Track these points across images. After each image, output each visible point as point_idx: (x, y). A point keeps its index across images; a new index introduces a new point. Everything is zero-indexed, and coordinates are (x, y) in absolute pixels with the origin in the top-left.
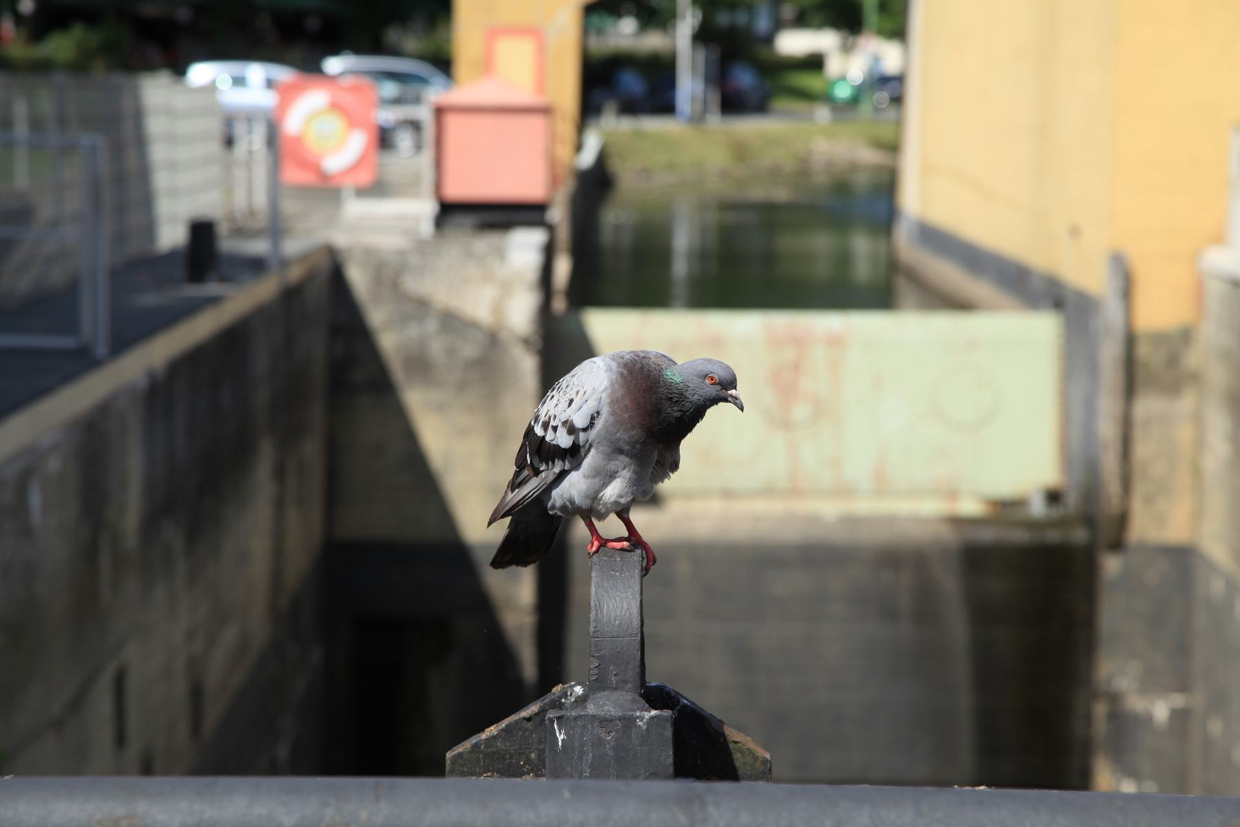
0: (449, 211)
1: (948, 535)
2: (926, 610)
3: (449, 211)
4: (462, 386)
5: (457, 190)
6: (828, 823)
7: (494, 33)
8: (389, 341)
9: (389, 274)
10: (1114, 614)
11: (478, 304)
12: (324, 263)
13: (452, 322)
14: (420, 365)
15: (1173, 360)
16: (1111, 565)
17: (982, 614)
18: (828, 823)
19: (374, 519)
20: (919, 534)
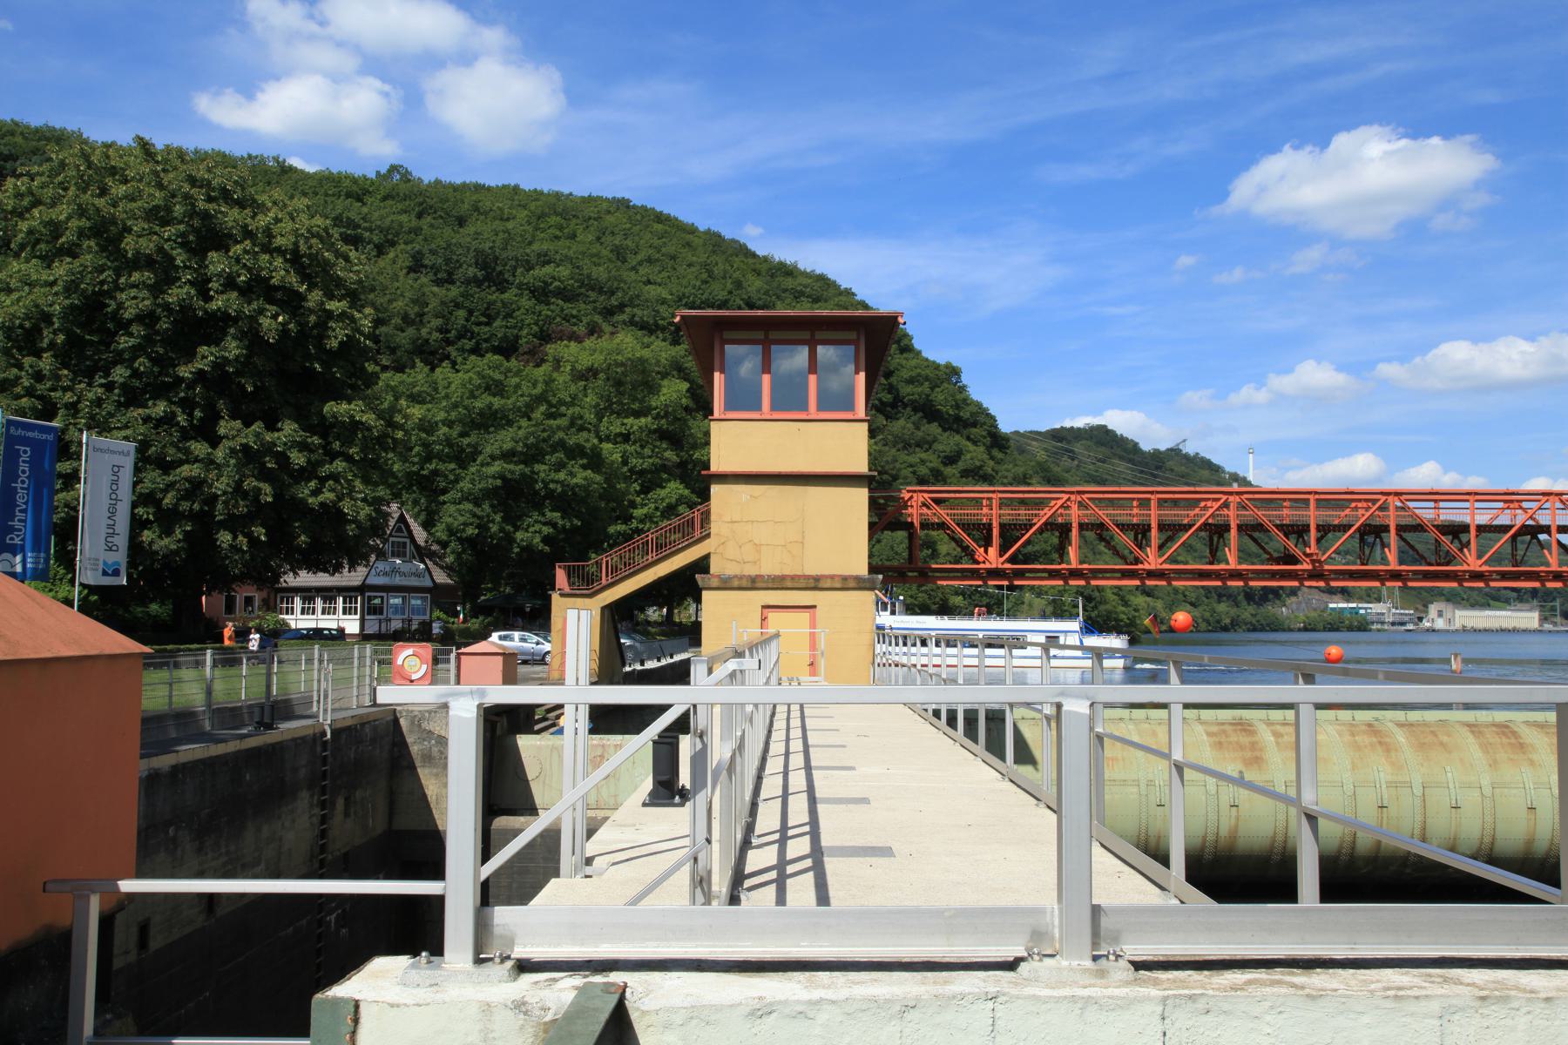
8: (415, 749)
19: (404, 822)
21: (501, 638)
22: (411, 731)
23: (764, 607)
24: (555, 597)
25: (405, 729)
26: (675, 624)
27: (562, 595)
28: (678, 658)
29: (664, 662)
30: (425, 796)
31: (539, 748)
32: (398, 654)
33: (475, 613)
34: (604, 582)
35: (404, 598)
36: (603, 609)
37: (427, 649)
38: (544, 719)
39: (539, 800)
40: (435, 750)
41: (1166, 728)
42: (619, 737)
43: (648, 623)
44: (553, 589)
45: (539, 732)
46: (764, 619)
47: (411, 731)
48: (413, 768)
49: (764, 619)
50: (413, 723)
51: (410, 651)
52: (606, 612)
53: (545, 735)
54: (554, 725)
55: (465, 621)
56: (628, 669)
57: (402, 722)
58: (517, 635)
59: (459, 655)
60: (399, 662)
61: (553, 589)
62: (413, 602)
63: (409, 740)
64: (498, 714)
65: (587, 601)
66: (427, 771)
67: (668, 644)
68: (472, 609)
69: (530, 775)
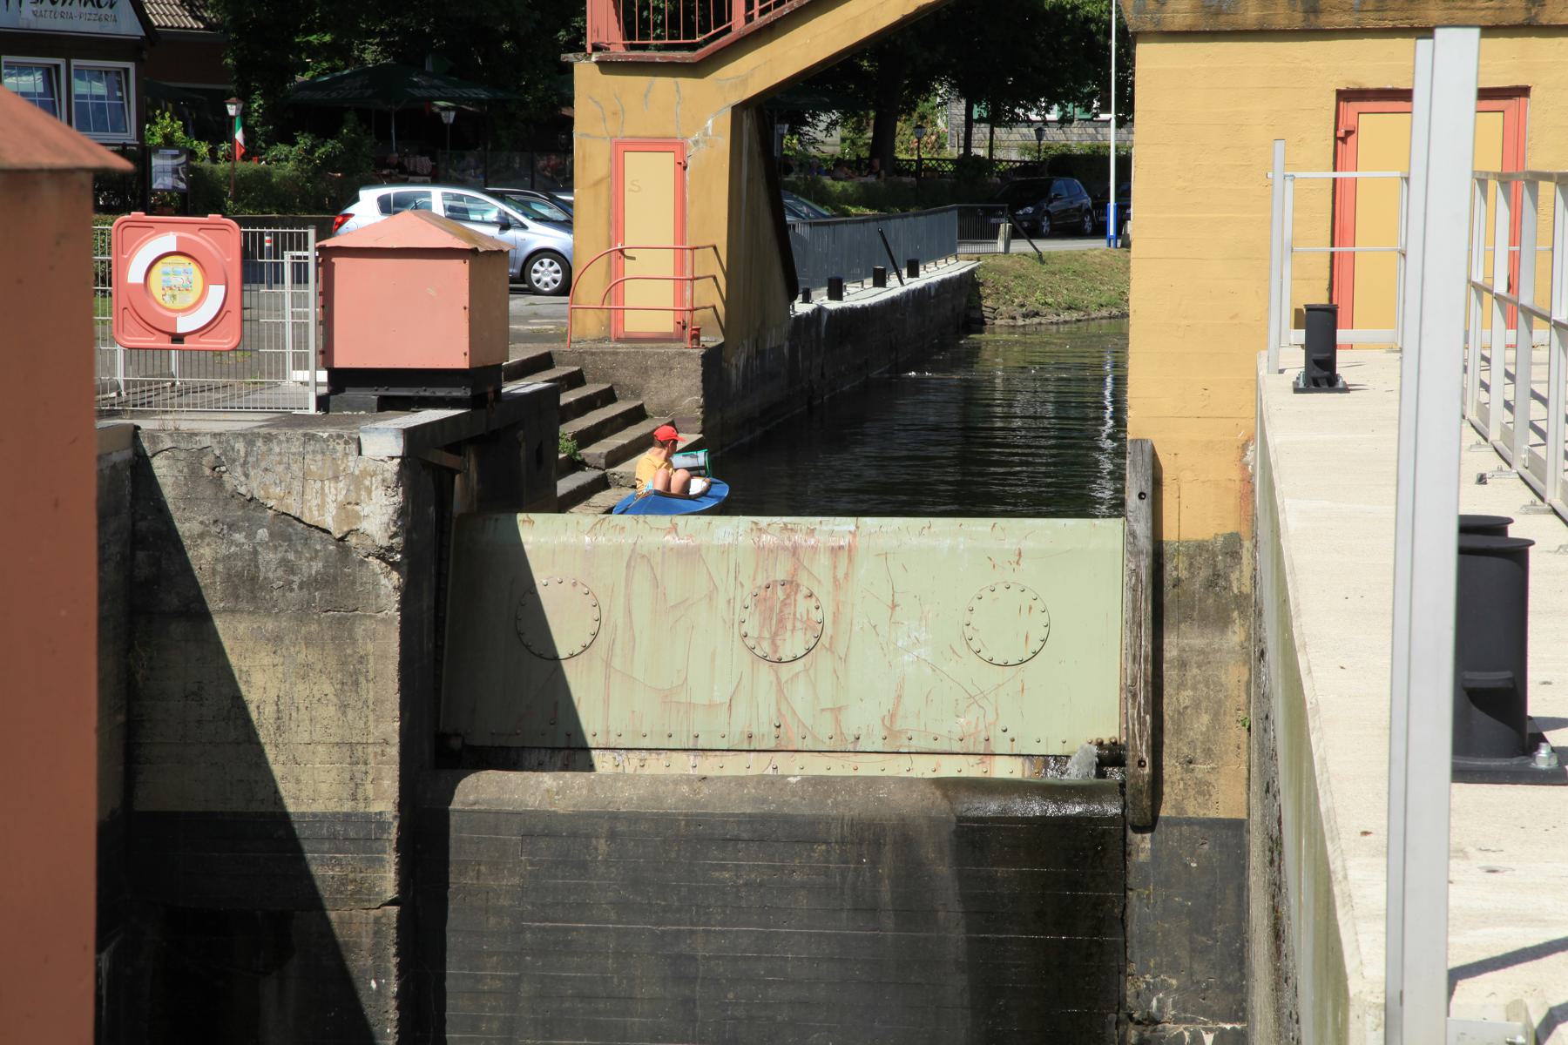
0: (342, 380)
1: (939, 804)
2: (913, 907)
3: (342, 380)
4: (303, 612)
5: (340, 362)
6: (1209, 1039)
7: (622, 147)
8: (203, 557)
9: (208, 469)
10: (1145, 909)
11: (322, 507)
12: (123, 455)
13: (290, 527)
14: (247, 585)
15: (1216, 580)
16: (1143, 844)
17: (983, 909)
18: (1209, 1039)
19: (175, 788)
20: (908, 804)
21: (386, 206)
22: (189, 500)
23: (1345, 96)
24: (585, 72)
25: (169, 492)
26: (898, 169)
27: (607, 66)
28: (935, 273)
29: (896, 287)
30: (238, 705)
31: (590, 554)
32: (131, 248)
33: (283, 123)
34: (738, 23)
35: (50, 74)
36: (739, 110)
37: (221, 237)
38: (575, 465)
39: (593, 721)
40: (269, 558)
41: (771, 745)
42: (847, 523)
43: (812, 166)
44: (576, 45)
45: (564, 505)
46: (1343, 137)
47: (189, 500)
48: (197, 615)
49: (1343, 137)
50: (194, 473)
51: (167, 241)
52: (747, 123)
53: (580, 517)
54: (602, 484)
55: (251, 152)
56: (801, 308)
57: (161, 467)
58: (437, 197)
59: (326, 254)
60: (135, 275)
61: (576, 45)
62: (80, 87)
63: (186, 527)
64: (455, 448)
65: (687, 84)
66: (243, 625)
67: (904, 229)
68: (269, 114)
69: (565, 639)
